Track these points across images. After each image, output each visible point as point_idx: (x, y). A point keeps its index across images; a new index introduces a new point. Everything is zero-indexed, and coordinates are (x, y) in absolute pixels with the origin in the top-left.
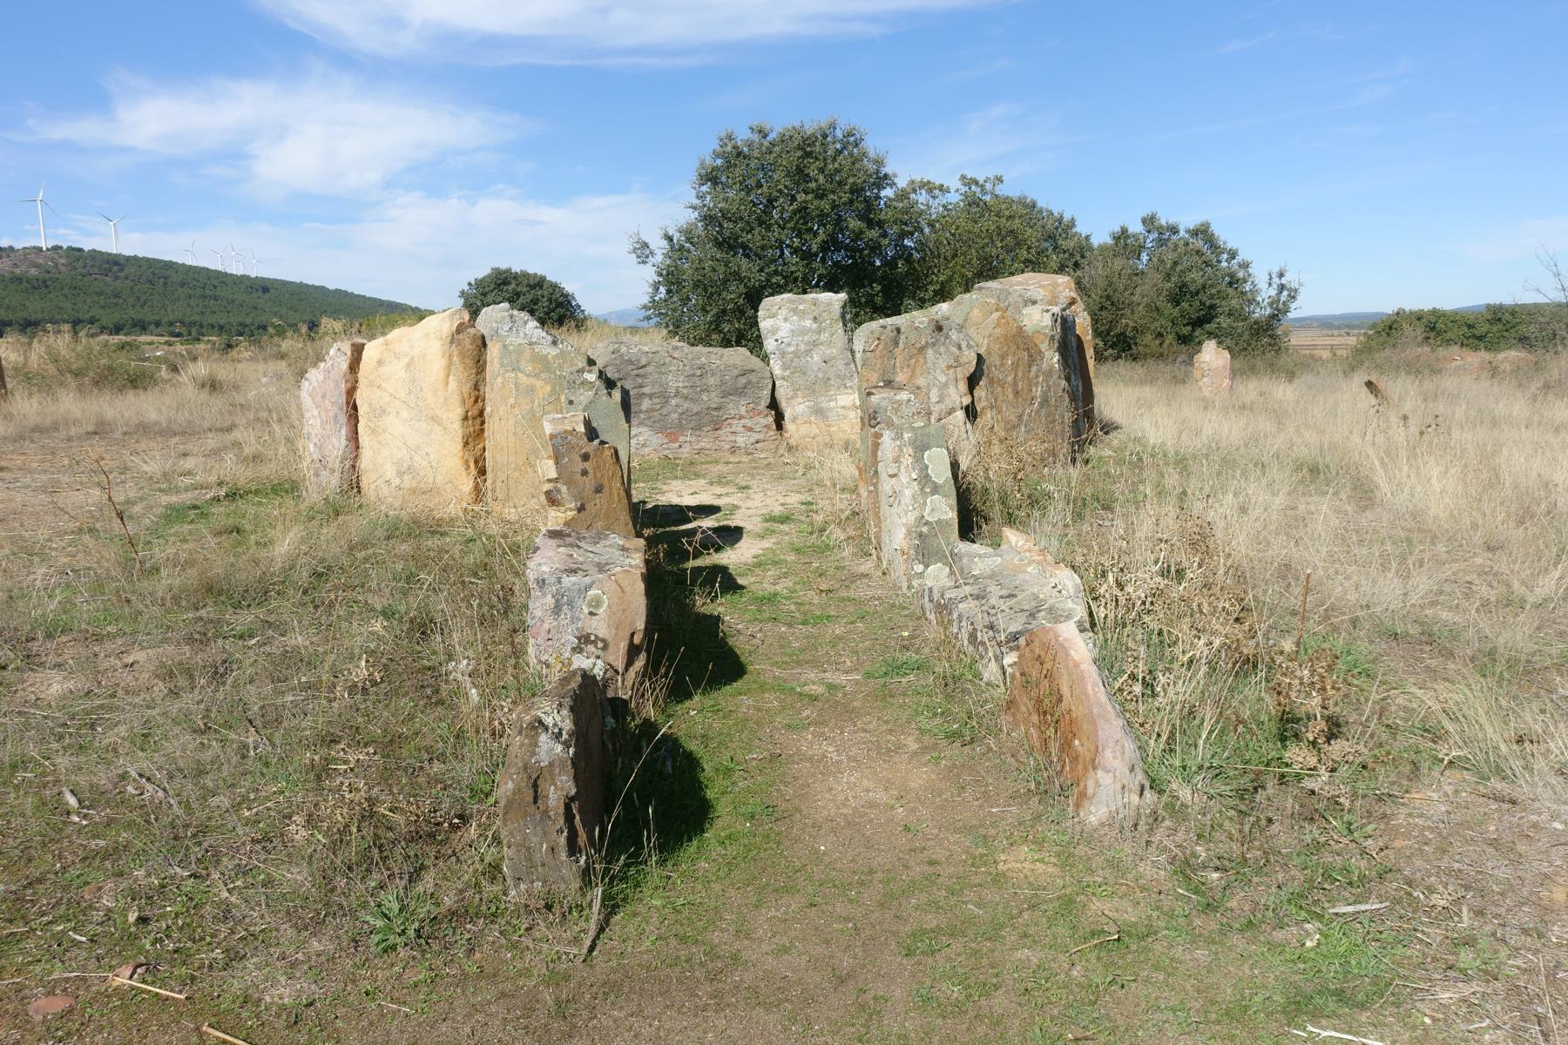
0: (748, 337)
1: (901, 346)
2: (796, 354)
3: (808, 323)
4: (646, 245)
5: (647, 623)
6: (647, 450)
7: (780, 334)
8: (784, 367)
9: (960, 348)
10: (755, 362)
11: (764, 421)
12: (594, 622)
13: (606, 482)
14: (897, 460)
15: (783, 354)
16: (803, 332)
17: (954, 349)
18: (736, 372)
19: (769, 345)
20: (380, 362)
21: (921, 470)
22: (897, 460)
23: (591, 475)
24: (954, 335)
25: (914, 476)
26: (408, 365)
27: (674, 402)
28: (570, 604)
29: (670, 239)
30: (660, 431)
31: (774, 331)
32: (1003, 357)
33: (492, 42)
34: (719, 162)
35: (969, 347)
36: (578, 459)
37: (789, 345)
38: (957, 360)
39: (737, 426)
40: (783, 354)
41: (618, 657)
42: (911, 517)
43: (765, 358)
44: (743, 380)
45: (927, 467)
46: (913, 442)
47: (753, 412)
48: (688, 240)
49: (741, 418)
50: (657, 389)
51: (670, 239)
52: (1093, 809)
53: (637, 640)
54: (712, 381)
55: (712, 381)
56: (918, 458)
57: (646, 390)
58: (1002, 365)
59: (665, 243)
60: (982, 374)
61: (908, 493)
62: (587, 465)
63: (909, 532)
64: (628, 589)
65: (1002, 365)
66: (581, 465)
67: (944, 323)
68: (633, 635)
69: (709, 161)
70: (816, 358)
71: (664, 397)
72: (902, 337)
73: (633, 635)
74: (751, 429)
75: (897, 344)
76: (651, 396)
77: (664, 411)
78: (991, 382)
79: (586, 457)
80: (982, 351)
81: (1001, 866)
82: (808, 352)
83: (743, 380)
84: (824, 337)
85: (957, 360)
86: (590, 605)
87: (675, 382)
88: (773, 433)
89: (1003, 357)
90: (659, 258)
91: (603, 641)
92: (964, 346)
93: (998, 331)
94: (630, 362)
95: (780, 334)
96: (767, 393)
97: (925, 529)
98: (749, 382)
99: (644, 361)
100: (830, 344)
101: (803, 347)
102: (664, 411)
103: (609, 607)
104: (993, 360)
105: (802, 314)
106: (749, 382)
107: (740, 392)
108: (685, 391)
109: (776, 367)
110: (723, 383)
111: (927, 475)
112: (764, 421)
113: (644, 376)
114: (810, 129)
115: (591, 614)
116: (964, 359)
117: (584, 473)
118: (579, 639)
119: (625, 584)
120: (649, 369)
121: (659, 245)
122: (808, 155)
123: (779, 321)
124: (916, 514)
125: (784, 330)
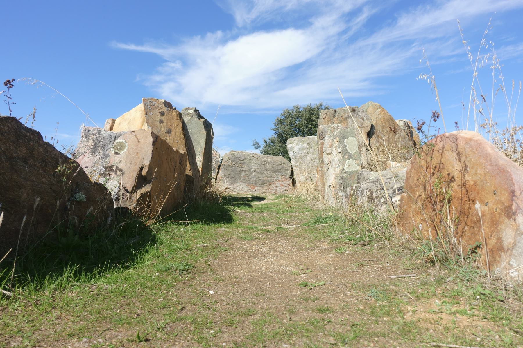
0: (285, 153)
1: (337, 117)
2: (301, 157)
3: (305, 145)
4: (258, 144)
5: (151, 162)
6: (243, 192)
7: (294, 150)
8: (296, 162)
9: (363, 120)
10: (286, 161)
11: (288, 183)
12: (117, 159)
13: (173, 129)
14: (331, 146)
15: (296, 157)
16: (304, 149)
17: (361, 120)
18: (278, 163)
19: (291, 154)
20: (120, 124)
21: (343, 147)
22: (331, 146)
23: (165, 124)
24: (361, 114)
25: (339, 151)
26: (129, 123)
27: (254, 174)
28: (104, 147)
29: (266, 142)
30: (249, 184)
31: (292, 148)
32: (383, 127)
33: (224, 107)
34: (283, 117)
35: (368, 119)
36: (165, 121)
37: (298, 153)
38: (362, 124)
39: (278, 184)
40: (296, 157)
41: (129, 182)
42: (338, 170)
43: (289, 160)
44: (280, 167)
45: (346, 146)
46: (339, 135)
47: (284, 179)
48: (272, 142)
49: (279, 181)
50: (248, 168)
51: (266, 142)
52: (513, 262)
53: (144, 173)
54: (268, 166)
55: (268, 166)
56: (341, 142)
57: (244, 169)
58: (383, 131)
59: (265, 144)
60: (374, 133)
61: (336, 159)
62: (163, 118)
63: (337, 176)
64: (142, 141)
65: (383, 131)
66: (159, 117)
67: (356, 109)
68: (141, 168)
69: (280, 118)
70: (308, 158)
71: (250, 172)
72: (337, 114)
73: (141, 168)
74: (283, 186)
75: (334, 116)
76: (245, 171)
77: (250, 177)
78: (378, 137)
79: (162, 114)
80: (373, 123)
81: (408, 317)
82: (305, 156)
83: (280, 167)
84: (311, 151)
85: (362, 124)
86: (116, 148)
87: (254, 166)
88: (291, 187)
89: (383, 127)
90: (262, 148)
91: (121, 170)
92: (365, 119)
93: (380, 116)
94: (238, 158)
95: (294, 150)
96: (289, 172)
97: (345, 175)
98: (283, 168)
99: (243, 158)
100: (314, 153)
101: (303, 154)
102: (250, 177)
103: (128, 150)
104: (378, 128)
105: (303, 142)
106: (283, 168)
107: (279, 171)
108: (258, 170)
109: (293, 163)
110: (273, 167)
111: (346, 150)
112: (288, 183)
113: (243, 164)
114: (313, 106)
115: (116, 153)
116: (365, 125)
117: (161, 122)
118: (106, 168)
119: (140, 137)
120: (245, 161)
121: (262, 144)
122: (312, 114)
123: (294, 145)
124: (340, 168)
125: (296, 148)
